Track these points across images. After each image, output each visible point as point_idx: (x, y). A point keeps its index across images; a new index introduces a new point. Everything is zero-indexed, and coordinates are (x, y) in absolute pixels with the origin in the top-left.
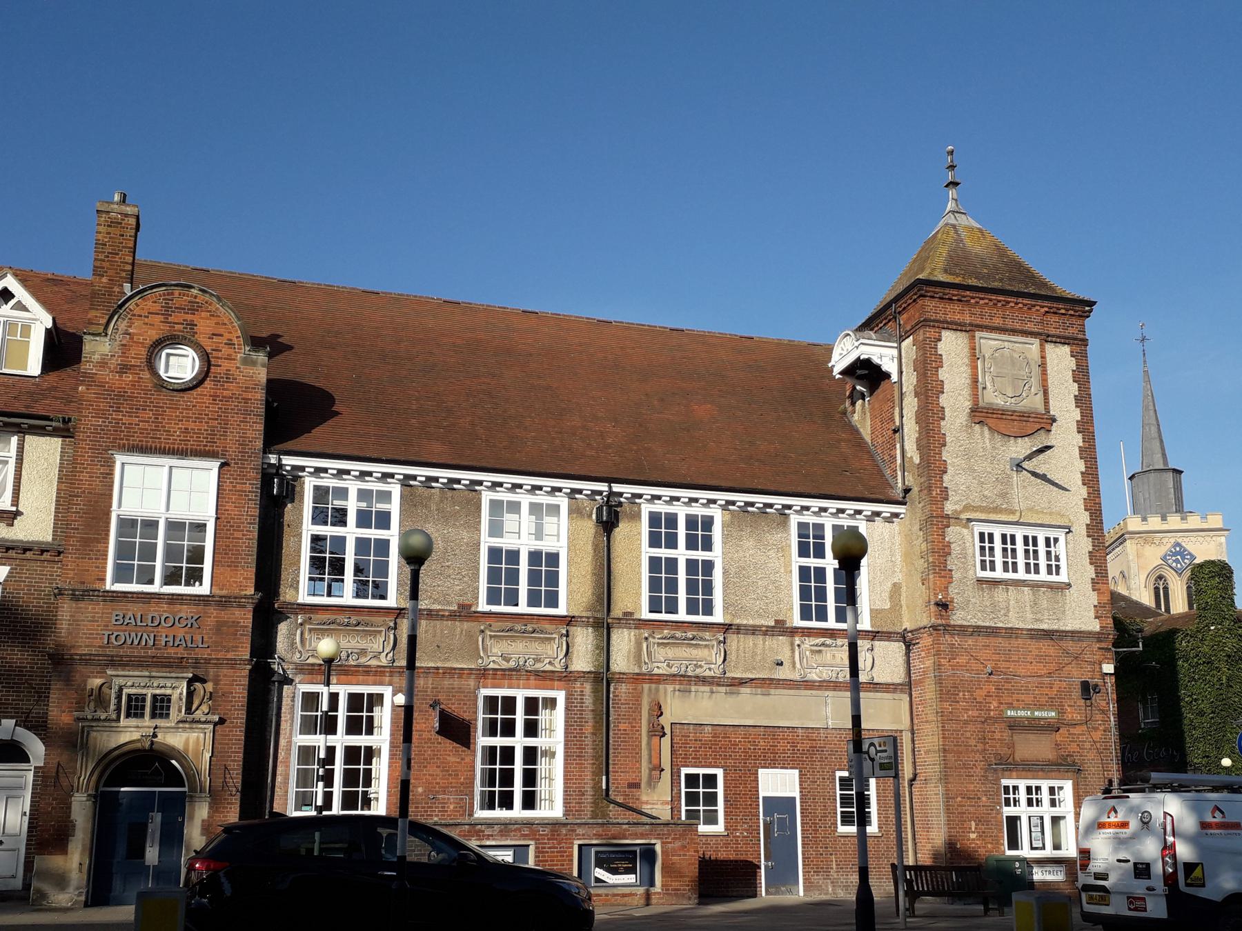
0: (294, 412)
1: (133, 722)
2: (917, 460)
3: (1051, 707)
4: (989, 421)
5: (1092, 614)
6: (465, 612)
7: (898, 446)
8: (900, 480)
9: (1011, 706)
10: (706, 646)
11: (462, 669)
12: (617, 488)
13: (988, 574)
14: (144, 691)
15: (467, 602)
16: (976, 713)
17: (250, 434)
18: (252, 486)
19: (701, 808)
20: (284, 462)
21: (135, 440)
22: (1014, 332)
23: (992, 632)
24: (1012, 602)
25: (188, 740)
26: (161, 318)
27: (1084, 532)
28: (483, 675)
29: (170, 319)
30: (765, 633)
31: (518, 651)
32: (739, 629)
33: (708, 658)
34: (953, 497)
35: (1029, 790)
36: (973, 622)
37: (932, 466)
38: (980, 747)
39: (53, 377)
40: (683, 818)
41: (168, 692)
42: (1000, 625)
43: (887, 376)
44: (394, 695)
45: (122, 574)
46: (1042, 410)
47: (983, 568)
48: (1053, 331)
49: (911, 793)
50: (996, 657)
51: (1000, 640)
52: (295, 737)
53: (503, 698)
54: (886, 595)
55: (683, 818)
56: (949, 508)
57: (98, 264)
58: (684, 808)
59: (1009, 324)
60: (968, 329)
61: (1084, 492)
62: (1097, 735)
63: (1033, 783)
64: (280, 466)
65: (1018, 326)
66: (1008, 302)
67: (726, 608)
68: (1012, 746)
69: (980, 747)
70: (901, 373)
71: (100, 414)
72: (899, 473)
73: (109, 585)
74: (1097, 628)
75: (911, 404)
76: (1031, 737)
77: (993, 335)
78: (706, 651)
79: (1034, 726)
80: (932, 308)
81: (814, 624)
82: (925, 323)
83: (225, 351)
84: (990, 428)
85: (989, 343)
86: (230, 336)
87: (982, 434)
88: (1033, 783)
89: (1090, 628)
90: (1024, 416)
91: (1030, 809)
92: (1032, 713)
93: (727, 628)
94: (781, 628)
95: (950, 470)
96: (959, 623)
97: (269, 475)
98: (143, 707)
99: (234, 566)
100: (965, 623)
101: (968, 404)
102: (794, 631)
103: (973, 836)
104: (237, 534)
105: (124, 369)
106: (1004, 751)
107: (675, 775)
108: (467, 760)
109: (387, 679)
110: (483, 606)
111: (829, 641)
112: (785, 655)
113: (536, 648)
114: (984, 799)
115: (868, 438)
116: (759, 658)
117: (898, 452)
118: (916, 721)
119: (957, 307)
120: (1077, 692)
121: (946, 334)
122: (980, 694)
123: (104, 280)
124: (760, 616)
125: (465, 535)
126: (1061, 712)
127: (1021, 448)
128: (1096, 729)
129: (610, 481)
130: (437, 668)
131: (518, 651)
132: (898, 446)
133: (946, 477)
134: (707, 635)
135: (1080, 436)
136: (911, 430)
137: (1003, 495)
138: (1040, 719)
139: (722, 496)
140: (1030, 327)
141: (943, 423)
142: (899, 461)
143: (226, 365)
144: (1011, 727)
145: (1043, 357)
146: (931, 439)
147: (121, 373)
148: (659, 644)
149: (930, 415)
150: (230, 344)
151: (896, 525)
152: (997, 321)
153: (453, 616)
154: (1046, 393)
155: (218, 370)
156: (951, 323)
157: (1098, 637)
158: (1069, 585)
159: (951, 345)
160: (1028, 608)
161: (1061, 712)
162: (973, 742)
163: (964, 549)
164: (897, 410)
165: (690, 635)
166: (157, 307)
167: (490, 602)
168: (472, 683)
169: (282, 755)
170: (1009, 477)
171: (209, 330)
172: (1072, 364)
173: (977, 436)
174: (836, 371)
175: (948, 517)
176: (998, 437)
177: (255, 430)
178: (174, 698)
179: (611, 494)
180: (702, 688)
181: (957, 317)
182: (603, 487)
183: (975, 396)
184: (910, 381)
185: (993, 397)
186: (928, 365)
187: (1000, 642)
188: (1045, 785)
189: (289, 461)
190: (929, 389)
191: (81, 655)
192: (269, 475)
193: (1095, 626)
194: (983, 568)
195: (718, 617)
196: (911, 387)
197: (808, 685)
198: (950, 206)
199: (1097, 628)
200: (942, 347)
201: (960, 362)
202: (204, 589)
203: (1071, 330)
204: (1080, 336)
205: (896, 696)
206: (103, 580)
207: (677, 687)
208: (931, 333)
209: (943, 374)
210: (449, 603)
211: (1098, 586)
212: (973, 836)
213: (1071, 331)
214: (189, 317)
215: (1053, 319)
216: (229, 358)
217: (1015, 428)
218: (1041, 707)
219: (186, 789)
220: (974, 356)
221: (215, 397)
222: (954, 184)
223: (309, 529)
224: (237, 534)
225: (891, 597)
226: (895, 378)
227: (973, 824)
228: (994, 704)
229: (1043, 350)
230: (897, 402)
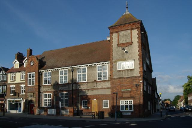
0: (42, 65)
3: (129, 89)
4: (121, 46)
9: (123, 89)
12: (72, 67)
18: (38, 73)
22: (125, 30)
23: (120, 78)
25: (34, 99)
32: (89, 82)
34: (114, 59)
35: (130, 101)
36: (117, 77)
39: (21, 67)
49: (150, 108)
52: (44, 99)
56: (113, 60)
59: (125, 29)
60: (117, 32)
62: (138, 92)
63: (126, 100)
65: (127, 29)
71: (27, 70)
79: (127, 92)
85: (121, 33)
88: (126, 100)
89: (138, 76)
93: (87, 82)
97: (39, 73)
99: (37, 82)
105: (28, 65)
113: (65, 88)
119: (116, 29)
120: (135, 86)
125: (58, 75)
126: (132, 89)
128: (138, 91)
129: (71, 66)
133: (113, 56)
138: (127, 91)
139: (86, 65)
140: (129, 28)
144: (122, 92)
151: (109, 64)
152: (123, 29)
157: (139, 77)
158: (134, 69)
161: (132, 89)
173: (119, 48)
175: (113, 62)
177: (38, 68)
182: (71, 67)
183: (118, 42)
187: (122, 80)
188: (129, 101)
189: (41, 71)
192: (39, 73)
193: (139, 75)
197: (98, 89)
198: (126, 11)
199: (140, 75)
200: (113, 36)
215: (133, 26)
218: (128, 89)
222: (128, 8)
223: (44, 77)
228: (120, 89)
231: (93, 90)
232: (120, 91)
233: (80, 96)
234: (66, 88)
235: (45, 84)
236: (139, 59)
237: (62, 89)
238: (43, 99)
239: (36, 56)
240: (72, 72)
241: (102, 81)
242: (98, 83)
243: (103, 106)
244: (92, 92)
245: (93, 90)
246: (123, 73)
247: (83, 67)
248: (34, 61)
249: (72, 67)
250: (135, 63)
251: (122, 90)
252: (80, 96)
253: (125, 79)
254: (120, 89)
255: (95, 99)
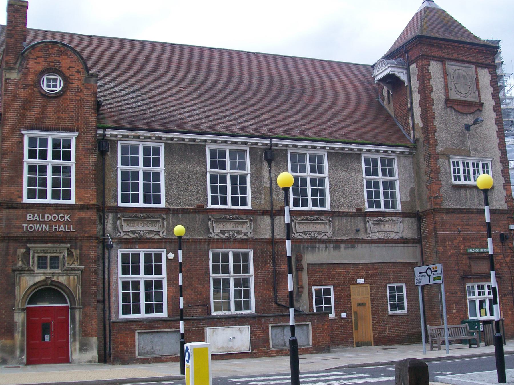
1: (42, 271)
2: (421, 125)
5: (504, 201)
6: (201, 210)
7: (410, 118)
8: (412, 136)
9: (470, 247)
10: (323, 223)
11: (201, 239)
13: (457, 182)
14: (46, 255)
15: (201, 204)
16: (454, 251)
17: (90, 119)
19: (323, 306)
20: (106, 133)
21: (33, 123)
22: (463, 61)
23: (460, 211)
24: (469, 196)
26: (43, 59)
27: (499, 160)
28: (211, 242)
29: (48, 60)
30: (351, 216)
31: (230, 229)
33: (326, 230)
35: (479, 287)
37: (428, 128)
38: (457, 268)
40: (315, 311)
41: (57, 255)
42: (464, 207)
43: (403, 82)
44: (167, 254)
45: (31, 194)
46: (477, 100)
47: (455, 179)
48: (481, 61)
50: (462, 223)
51: (463, 215)
53: (161, 265)
54: (408, 194)
55: (315, 311)
56: (439, 149)
57: (9, 32)
58: (314, 306)
59: (461, 58)
60: (442, 60)
61: (498, 141)
63: (481, 284)
64: (104, 135)
65: (464, 58)
66: (460, 47)
67: (331, 203)
68: (470, 267)
69: (457, 268)
70: (410, 80)
72: (412, 132)
73: (26, 200)
74: (507, 208)
75: (417, 98)
76: (480, 262)
77: (453, 63)
78: (323, 226)
80: (426, 50)
81: (374, 210)
82: (422, 57)
83: (77, 76)
84: (455, 109)
85: (452, 68)
86: (78, 68)
87: (451, 112)
88: (481, 284)
90: (470, 104)
91: (480, 297)
92: (479, 250)
94: (360, 213)
95: (438, 130)
96: (445, 207)
98: (46, 263)
100: (448, 207)
101: (443, 97)
102: (366, 215)
103: (454, 311)
104: (87, 172)
105: (26, 87)
106: (467, 269)
107: (310, 290)
108: (206, 286)
109: (163, 246)
110: (210, 206)
111: (382, 219)
112: (361, 226)
114: (459, 293)
115: (393, 114)
116: (348, 228)
117: (411, 121)
118: (424, 257)
121: (432, 62)
122: (456, 242)
123: (13, 40)
124: (349, 207)
127: (469, 120)
130: (189, 239)
131: (230, 229)
132: (410, 118)
133: (436, 134)
134: (323, 218)
135: (492, 89)
136: (417, 110)
137: (463, 143)
140: (470, 59)
141: (433, 107)
142: (411, 125)
143: (76, 83)
144: (470, 258)
145: (477, 74)
146: (427, 115)
147: (24, 88)
148: (299, 223)
149: (426, 103)
150: (78, 72)
152: (455, 56)
153: (195, 212)
154: (479, 92)
155: (73, 86)
156: (434, 57)
159: (434, 68)
160: (476, 199)
162: (453, 266)
163: (446, 170)
164: (409, 100)
165: (315, 218)
166: (40, 54)
167: (213, 204)
168: (206, 246)
169: (113, 285)
170: (464, 134)
171: (68, 65)
172: (490, 78)
174: (377, 79)
175: (437, 154)
176: (458, 114)
178: (61, 257)
179: (271, 145)
180: (321, 245)
181: (437, 54)
182: (267, 141)
183: (447, 94)
184: (415, 85)
185: (454, 96)
186: (424, 78)
187: (465, 216)
190: (425, 90)
191: (13, 237)
194: (455, 179)
195: (328, 208)
196: (416, 89)
199: (507, 208)
201: (439, 76)
202: (72, 201)
203: (488, 61)
204: (493, 64)
205: (414, 245)
206: (21, 197)
207: (309, 245)
208: (425, 62)
209: (432, 82)
210: (192, 205)
211: (506, 187)
212: (454, 311)
213: (489, 61)
214: (57, 58)
216: (78, 80)
217: (465, 110)
219: (69, 305)
220: (445, 74)
221: (72, 100)
224: (87, 172)
225: (410, 195)
226: (406, 84)
227: (454, 305)
229: (476, 71)
230: (409, 95)
231: (353, 247)
232: (462, 254)
233: (305, 267)
234: (243, 228)
235: (125, 199)
236: (500, 157)
237: (223, 233)
238: (113, 279)
239: (483, 121)
240: (269, 162)
241: (383, 214)
242: (372, 220)
243: (246, 312)
244: (350, 251)
245: (352, 243)
246: (466, 195)
247: (313, 152)
248: (67, 73)
249: (275, 142)
250: (494, 167)
251: (470, 251)
252: (305, 267)
253: (473, 215)
254: (462, 247)
255: (362, 281)
